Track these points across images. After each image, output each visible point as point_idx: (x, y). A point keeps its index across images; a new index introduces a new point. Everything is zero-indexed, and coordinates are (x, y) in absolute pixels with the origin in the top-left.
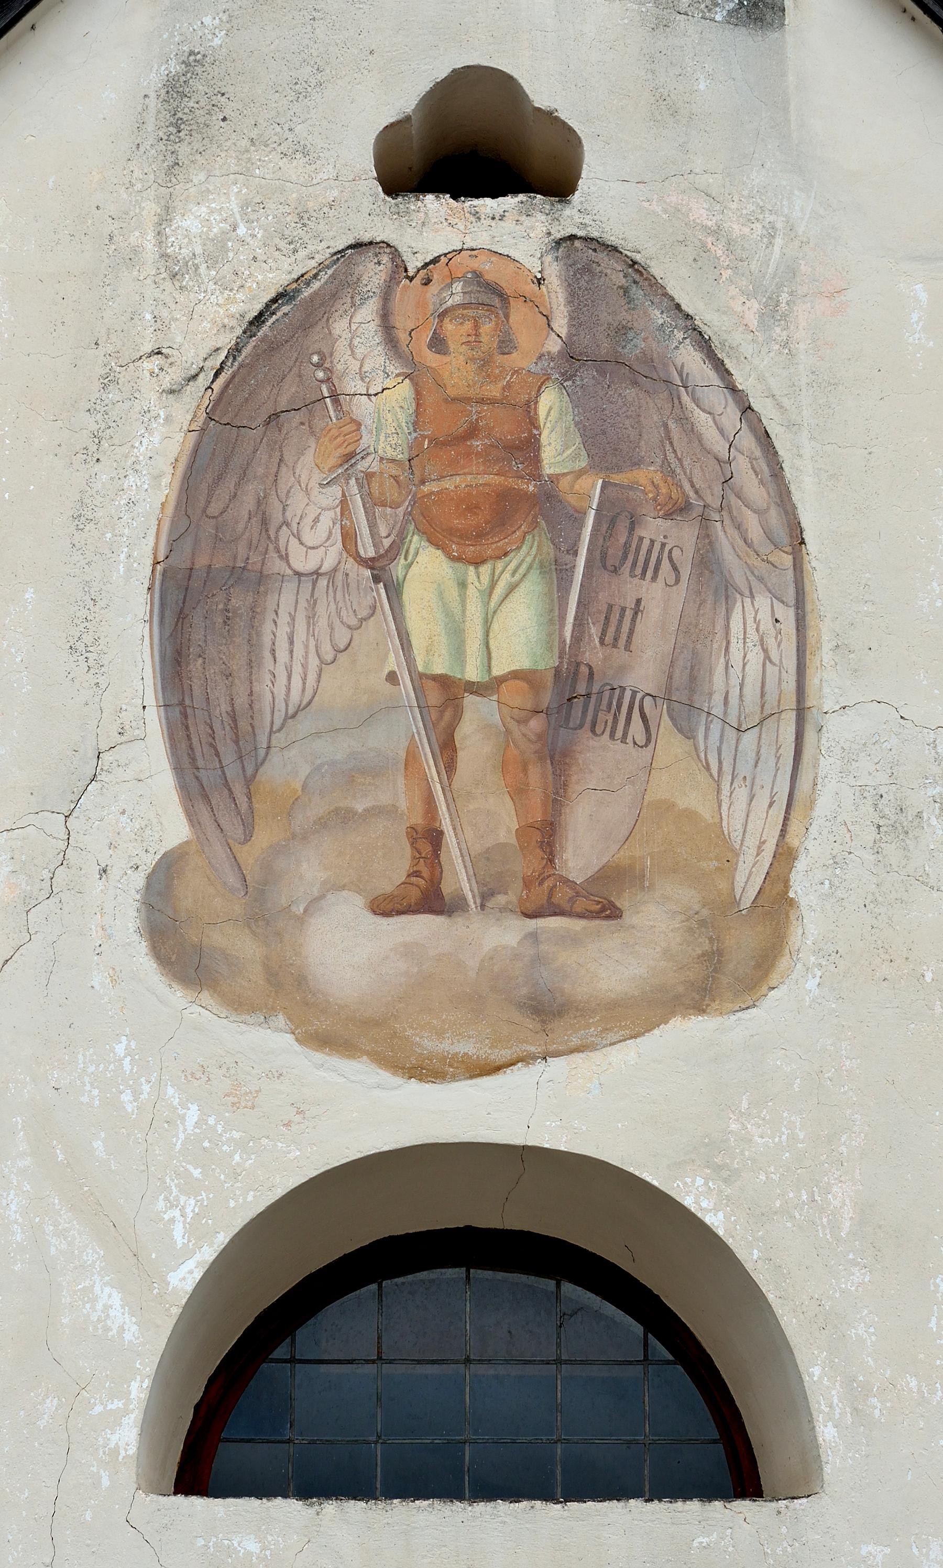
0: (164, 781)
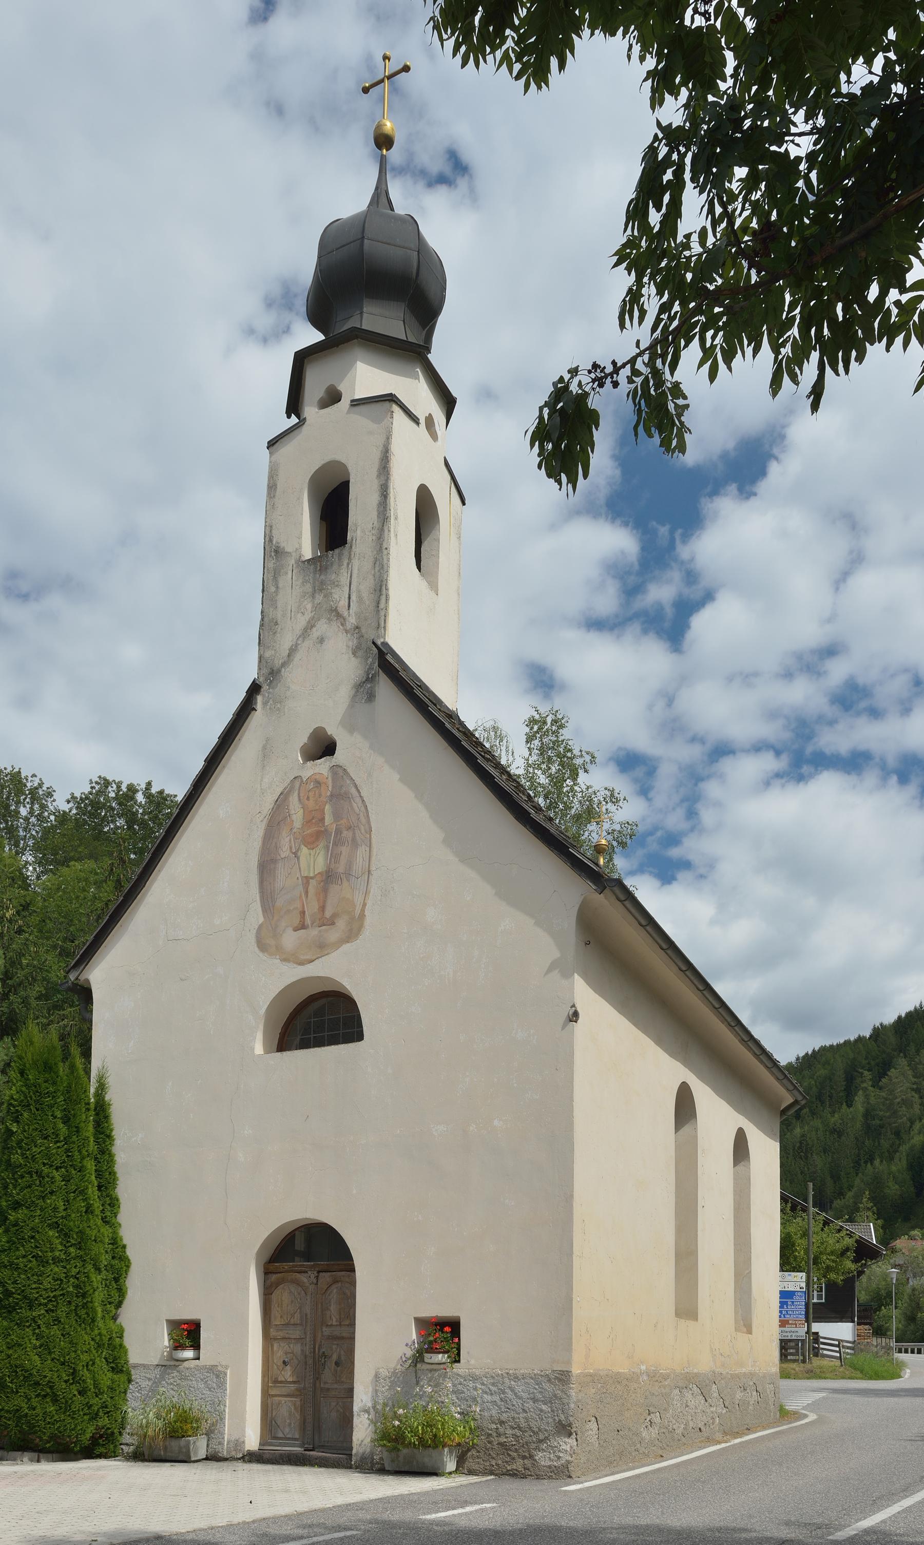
0: (260, 910)
